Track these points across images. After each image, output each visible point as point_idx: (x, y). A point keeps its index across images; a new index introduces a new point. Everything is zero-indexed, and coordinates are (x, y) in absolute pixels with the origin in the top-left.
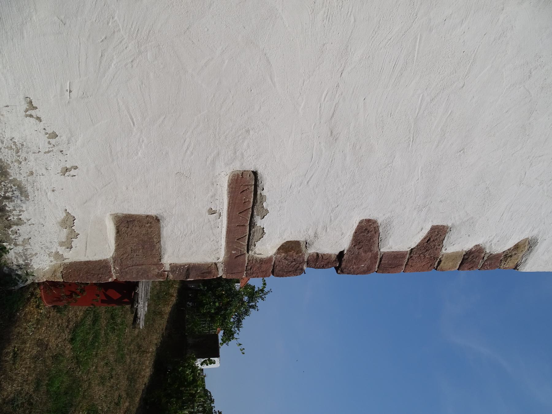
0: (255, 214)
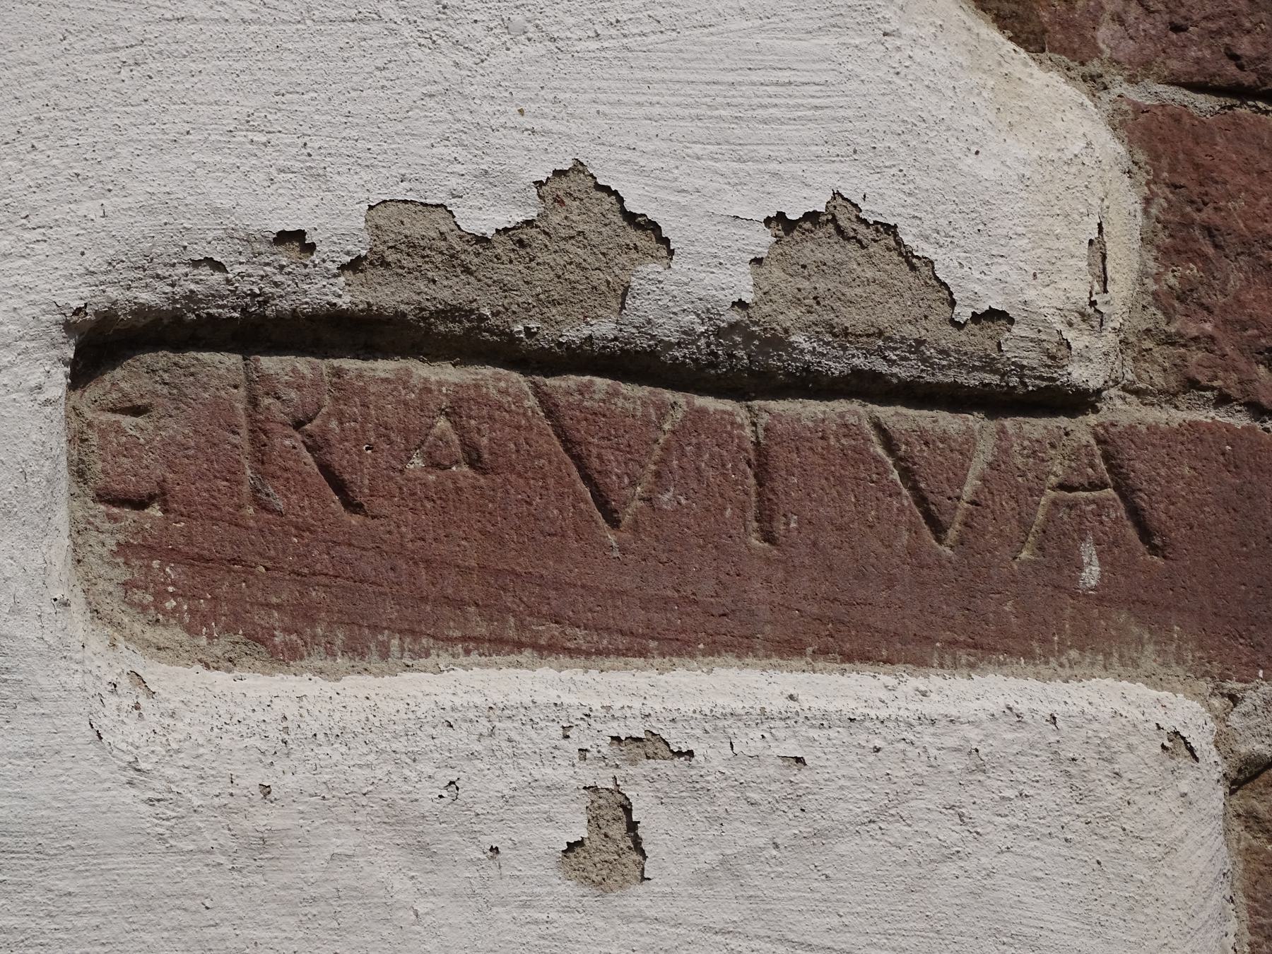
0: (604, 328)
